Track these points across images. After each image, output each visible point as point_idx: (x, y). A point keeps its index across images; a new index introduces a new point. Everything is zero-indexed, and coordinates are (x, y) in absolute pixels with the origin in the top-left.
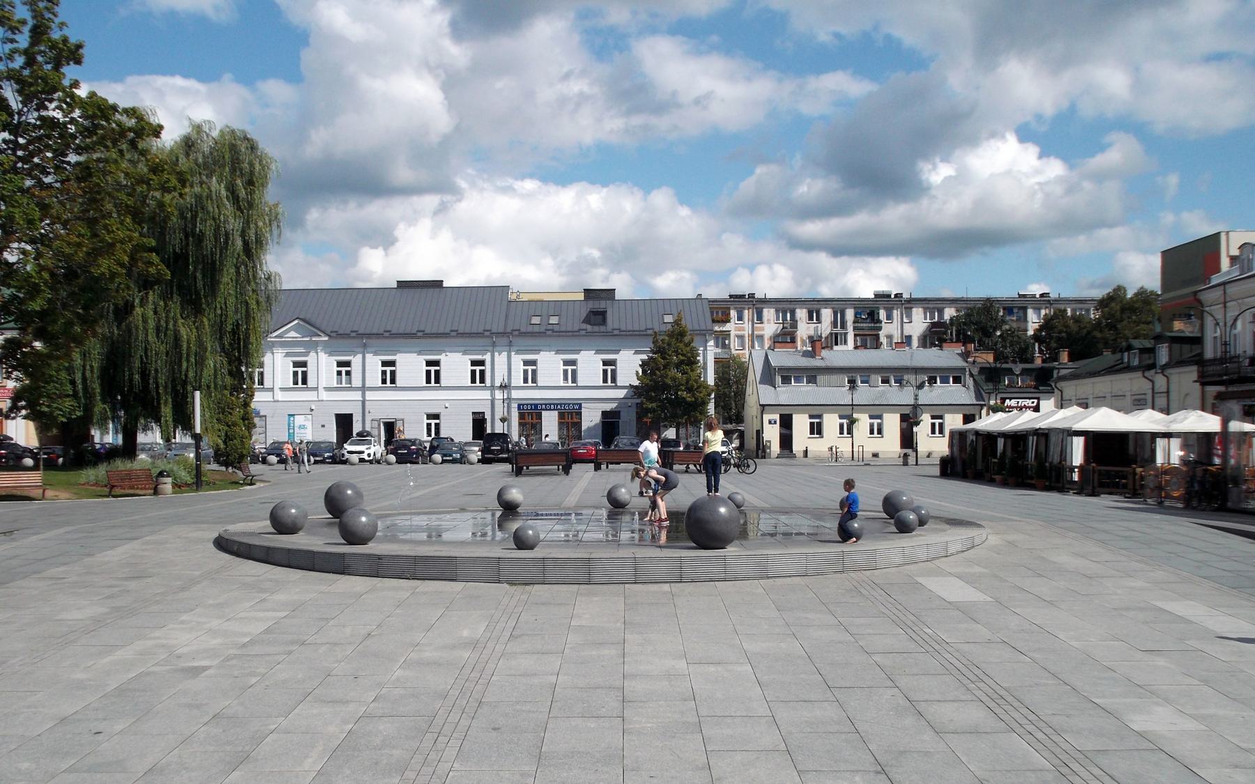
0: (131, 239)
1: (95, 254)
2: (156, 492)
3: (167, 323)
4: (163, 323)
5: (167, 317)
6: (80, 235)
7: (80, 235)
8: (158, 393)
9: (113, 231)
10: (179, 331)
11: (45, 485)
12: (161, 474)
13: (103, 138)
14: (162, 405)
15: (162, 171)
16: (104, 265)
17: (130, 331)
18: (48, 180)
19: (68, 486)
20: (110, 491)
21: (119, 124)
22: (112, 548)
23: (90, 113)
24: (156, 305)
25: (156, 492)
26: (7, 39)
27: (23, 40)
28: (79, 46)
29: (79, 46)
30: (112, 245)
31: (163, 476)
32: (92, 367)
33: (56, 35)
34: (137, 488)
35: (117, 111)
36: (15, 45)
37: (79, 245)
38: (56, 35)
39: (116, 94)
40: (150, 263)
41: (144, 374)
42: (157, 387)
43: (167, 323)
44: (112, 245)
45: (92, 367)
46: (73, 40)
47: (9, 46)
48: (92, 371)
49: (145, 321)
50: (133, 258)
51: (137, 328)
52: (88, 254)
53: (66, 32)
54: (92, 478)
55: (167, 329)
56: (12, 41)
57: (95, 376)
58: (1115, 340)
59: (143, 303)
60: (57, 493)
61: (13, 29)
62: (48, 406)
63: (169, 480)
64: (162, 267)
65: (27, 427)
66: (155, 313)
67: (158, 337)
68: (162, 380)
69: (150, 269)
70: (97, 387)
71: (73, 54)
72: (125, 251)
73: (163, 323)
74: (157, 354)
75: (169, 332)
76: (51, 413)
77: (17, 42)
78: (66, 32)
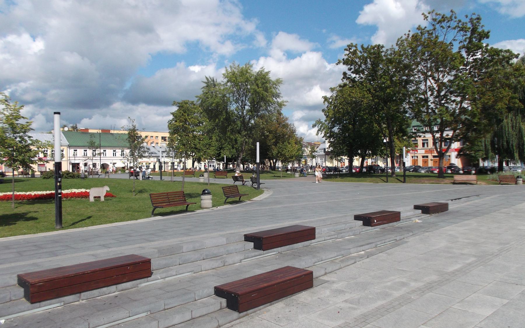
0: (509, 95)
1: (496, 102)
2: (516, 183)
3: (516, 124)
4: (514, 124)
5: (516, 122)
6: (489, 96)
7: (489, 96)
8: (513, 149)
9: (503, 93)
10: (521, 127)
11: (477, 180)
12: (518, 177)
13: (496, 62)
14: (515, 153)
15: (519, 70)
16: (500, 105)
17: (502, 127)
18: (476, 79)
19: (483, 180)
20: (500, 182)
21: (503, 56)
22: (520, 203)
23: (493, 54)
24: (512, 118)
25: (516, 183)
26: (464, 35)
27: (469, 34)
28: (488, 32)
29: (488, 32)
30: (502, 98)
31: (519, 178)
32: (488, 141)
33: (480, 30)
34: (508, 182)
35: (502, 52)
36: (467, 36)
37: (490, 99)
38: (480, 30)
39: (495, 47)
40: (515, 103)
41: (508, 142)
42: (513, 147)
43: (516, 124)
44: (502, 98)
45: (488, 141)
46: (486, 31)
47: (465, 37)
48: (488, 142)
49: (508, 124)
50: (509, 101)
51: (505, 126)
52: (493, 102)
53: (484, 28)
54: (491, 178)
55: (516, 126)
56: (466, 35)
57: (489, 143)
58: (170, 151)
59: (507, 117)
60: (481, 183)
61: (466, 32)
62: (474, 154)
63: (521, 179)
64: (520, 104)
65: (458, 161)
66: (511, 121)
67: (512, 129)
68: (514, 144)
69: (516, 105)
70: (490, 148)
71: (486, 35)
72: (507, 100)
73: (514, 124)
74: (512, 135)
75: (517, 127)
76: (476, 156)
77: (467, 35)
78: (484, 28)
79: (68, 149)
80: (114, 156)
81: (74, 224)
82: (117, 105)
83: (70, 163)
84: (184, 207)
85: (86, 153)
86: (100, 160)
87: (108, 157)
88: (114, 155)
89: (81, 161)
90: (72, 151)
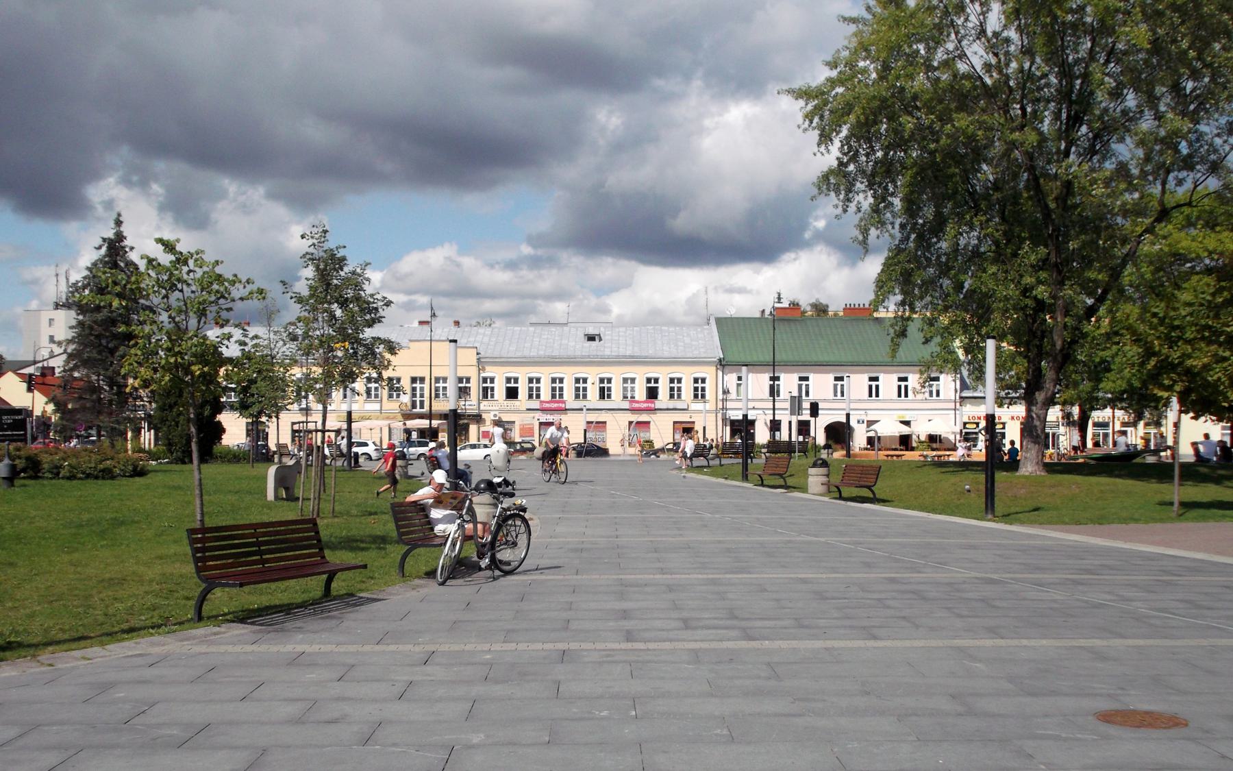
79: (720, 373)
80: (835, 395)
81: (1007, 517)
82: (1121, 158)
83: (724, 420)
84: (314, 585)
85: (807, 386)
86: (774, 409)
87: (884, 401)
88: (874, 392)
89: (761, 412)
90: (731, 379)
